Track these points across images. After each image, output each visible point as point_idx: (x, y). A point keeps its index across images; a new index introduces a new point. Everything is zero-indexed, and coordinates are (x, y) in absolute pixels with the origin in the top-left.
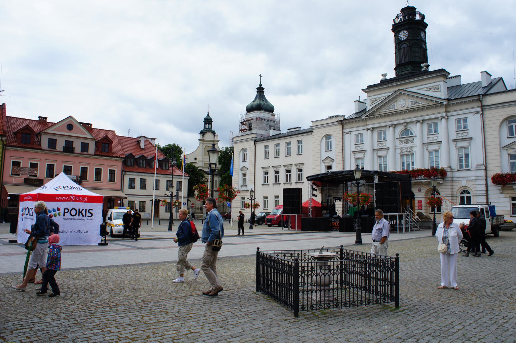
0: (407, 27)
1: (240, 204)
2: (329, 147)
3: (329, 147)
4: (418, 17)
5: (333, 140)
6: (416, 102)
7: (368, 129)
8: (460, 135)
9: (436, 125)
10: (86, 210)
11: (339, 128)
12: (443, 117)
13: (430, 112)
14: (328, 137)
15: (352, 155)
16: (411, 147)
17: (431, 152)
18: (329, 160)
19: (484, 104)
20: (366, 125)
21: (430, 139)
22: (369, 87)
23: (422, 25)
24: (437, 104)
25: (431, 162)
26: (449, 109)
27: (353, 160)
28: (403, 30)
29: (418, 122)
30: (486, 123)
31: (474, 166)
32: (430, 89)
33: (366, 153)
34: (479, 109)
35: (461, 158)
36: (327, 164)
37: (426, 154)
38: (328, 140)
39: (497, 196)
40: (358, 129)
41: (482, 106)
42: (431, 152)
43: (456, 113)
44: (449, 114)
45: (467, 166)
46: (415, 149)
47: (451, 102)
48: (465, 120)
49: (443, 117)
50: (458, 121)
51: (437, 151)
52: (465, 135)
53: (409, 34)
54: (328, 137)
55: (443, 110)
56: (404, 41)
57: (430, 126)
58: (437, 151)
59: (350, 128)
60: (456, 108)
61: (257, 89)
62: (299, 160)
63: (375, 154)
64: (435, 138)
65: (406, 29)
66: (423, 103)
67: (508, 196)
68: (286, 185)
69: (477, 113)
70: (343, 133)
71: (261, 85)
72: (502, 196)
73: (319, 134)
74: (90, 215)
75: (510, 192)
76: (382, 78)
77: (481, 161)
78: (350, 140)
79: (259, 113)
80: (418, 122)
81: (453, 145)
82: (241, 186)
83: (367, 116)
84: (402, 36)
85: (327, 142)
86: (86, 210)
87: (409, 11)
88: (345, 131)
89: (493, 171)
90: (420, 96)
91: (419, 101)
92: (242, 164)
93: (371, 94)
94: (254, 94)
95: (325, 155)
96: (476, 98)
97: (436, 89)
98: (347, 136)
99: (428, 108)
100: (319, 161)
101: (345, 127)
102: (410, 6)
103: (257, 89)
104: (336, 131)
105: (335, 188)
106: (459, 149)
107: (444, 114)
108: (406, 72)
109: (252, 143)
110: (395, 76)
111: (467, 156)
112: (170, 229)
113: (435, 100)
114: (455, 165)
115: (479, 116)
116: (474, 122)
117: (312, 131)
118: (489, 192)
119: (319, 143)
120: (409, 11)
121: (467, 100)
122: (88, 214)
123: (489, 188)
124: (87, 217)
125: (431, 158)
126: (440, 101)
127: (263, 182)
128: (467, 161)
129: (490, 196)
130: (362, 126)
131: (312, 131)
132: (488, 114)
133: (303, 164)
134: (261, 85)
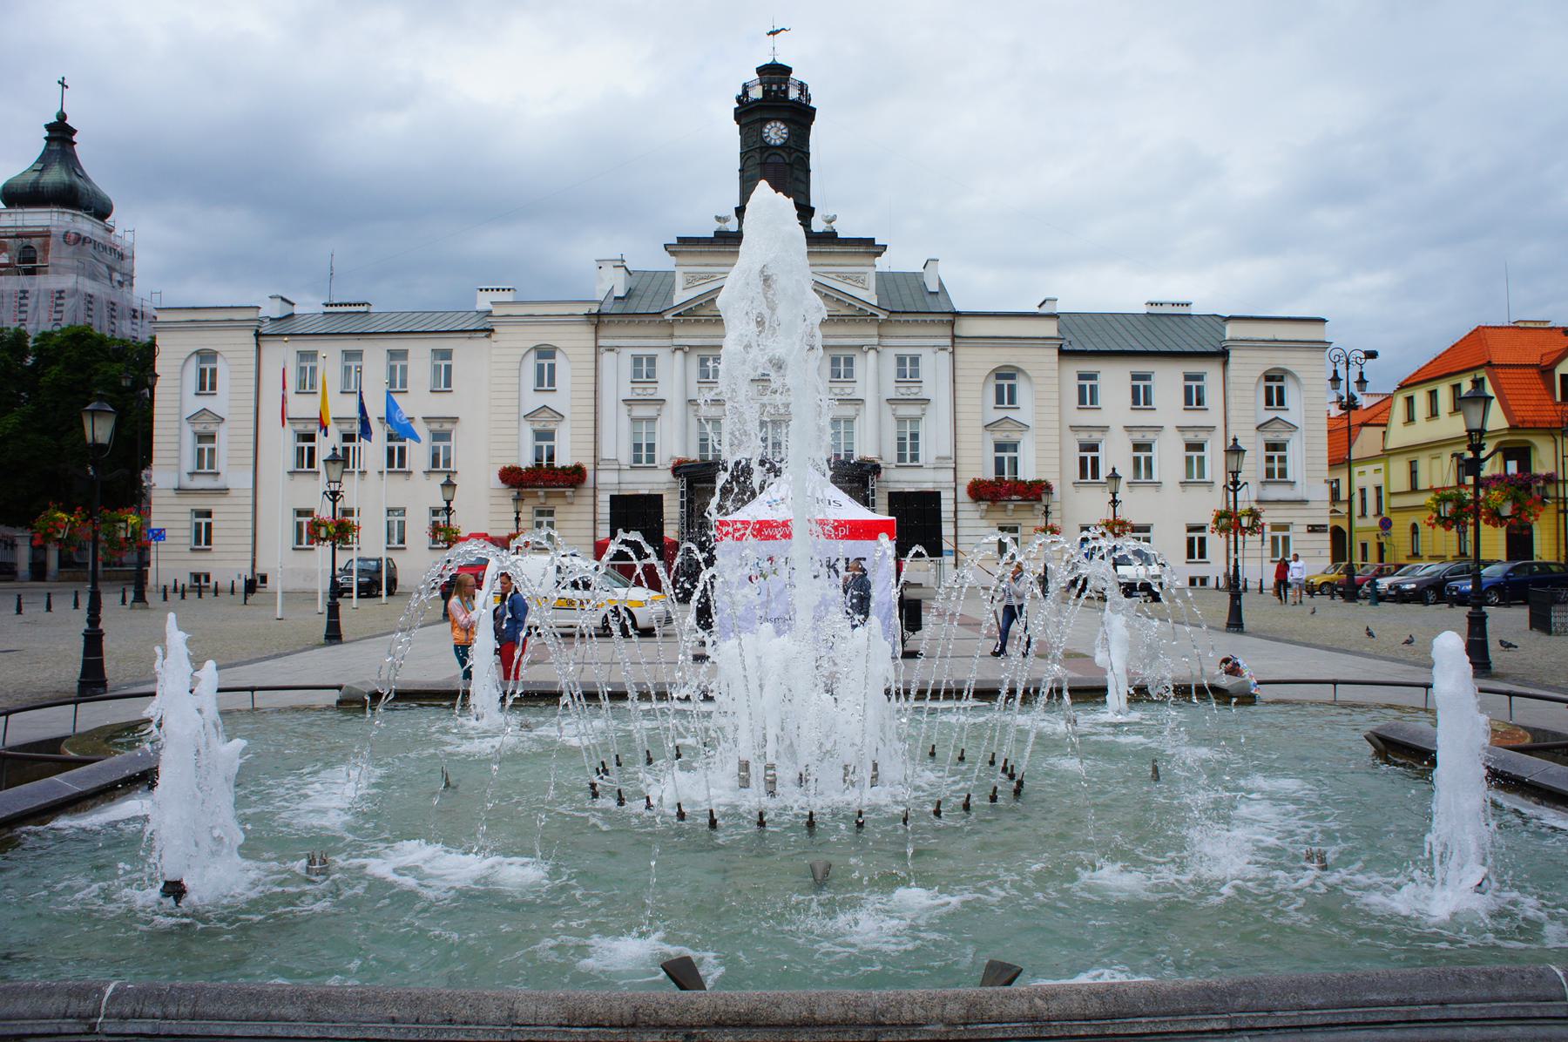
0: (786, 115)
1: (187, 533)
3: (546, 379)
4: (793, 94)
5: (220, 365)
7: (680, 348)
9: (849, 361)
14: (207, 356)
15: (624, 408)
19: (957, 332)
20: (671, 336)
22: (683, 241)
23: (801, 115)
26: (885, 331)
27: (625, 423)
28: (776, 120)
30: (958, 372)
31: (932, 459)
32: (845, 278)
33: (665, 409)
34: (948, 342)
35: (901, 439)
36: (538, 426)
41: (954, 337)
43: (904, 342)
44: (886, 341)
45: (915, 457)
48: (915, 360)
49: (872, 348)
53: (789, 133)
54: (545, 352)
55: (873, 331)
61: (49, 127)
62: (441, 406)
63: (691, 414)
65: (783, 121)
68: (197, 478)
69: (943, 349)
70: (597, 347)
71: (62, 117)
72: (984, 523)
73: (514, 343)
76: (717, 226)
77: (947, 451)
79: (68, 218)
81: (887, 408)
82: (192, 474)
83: (679, 315)
84: (772, 134)
87: (775, 74)
92: (194, 404)
93: (683, 260)
94: (36, 143)
95: (533, 401)
97: (858, 280)
98: (607, 359)
100: (515, 417)
101: (601, 333)
102: (779, 61)
103: (49, 127)
104: (574, 344)
105: (569, 491)
107: (875, 341)
109: (249, 337)
111: (915, 436)
112: (76, 605)
114: (890, 454)
115: (945, 356)
116: (934, 366)
117: (489, 331)
118: (960, 515)
120: (775, 74)
121: (929, 318)
123: (960, 507)
125: (836, 435)
126: (870, 311)
127: (291, 466)
128: (915, 447)
129: (960, 523)
132: (963, 353)
133: (455, 420)
134: (62, 117)
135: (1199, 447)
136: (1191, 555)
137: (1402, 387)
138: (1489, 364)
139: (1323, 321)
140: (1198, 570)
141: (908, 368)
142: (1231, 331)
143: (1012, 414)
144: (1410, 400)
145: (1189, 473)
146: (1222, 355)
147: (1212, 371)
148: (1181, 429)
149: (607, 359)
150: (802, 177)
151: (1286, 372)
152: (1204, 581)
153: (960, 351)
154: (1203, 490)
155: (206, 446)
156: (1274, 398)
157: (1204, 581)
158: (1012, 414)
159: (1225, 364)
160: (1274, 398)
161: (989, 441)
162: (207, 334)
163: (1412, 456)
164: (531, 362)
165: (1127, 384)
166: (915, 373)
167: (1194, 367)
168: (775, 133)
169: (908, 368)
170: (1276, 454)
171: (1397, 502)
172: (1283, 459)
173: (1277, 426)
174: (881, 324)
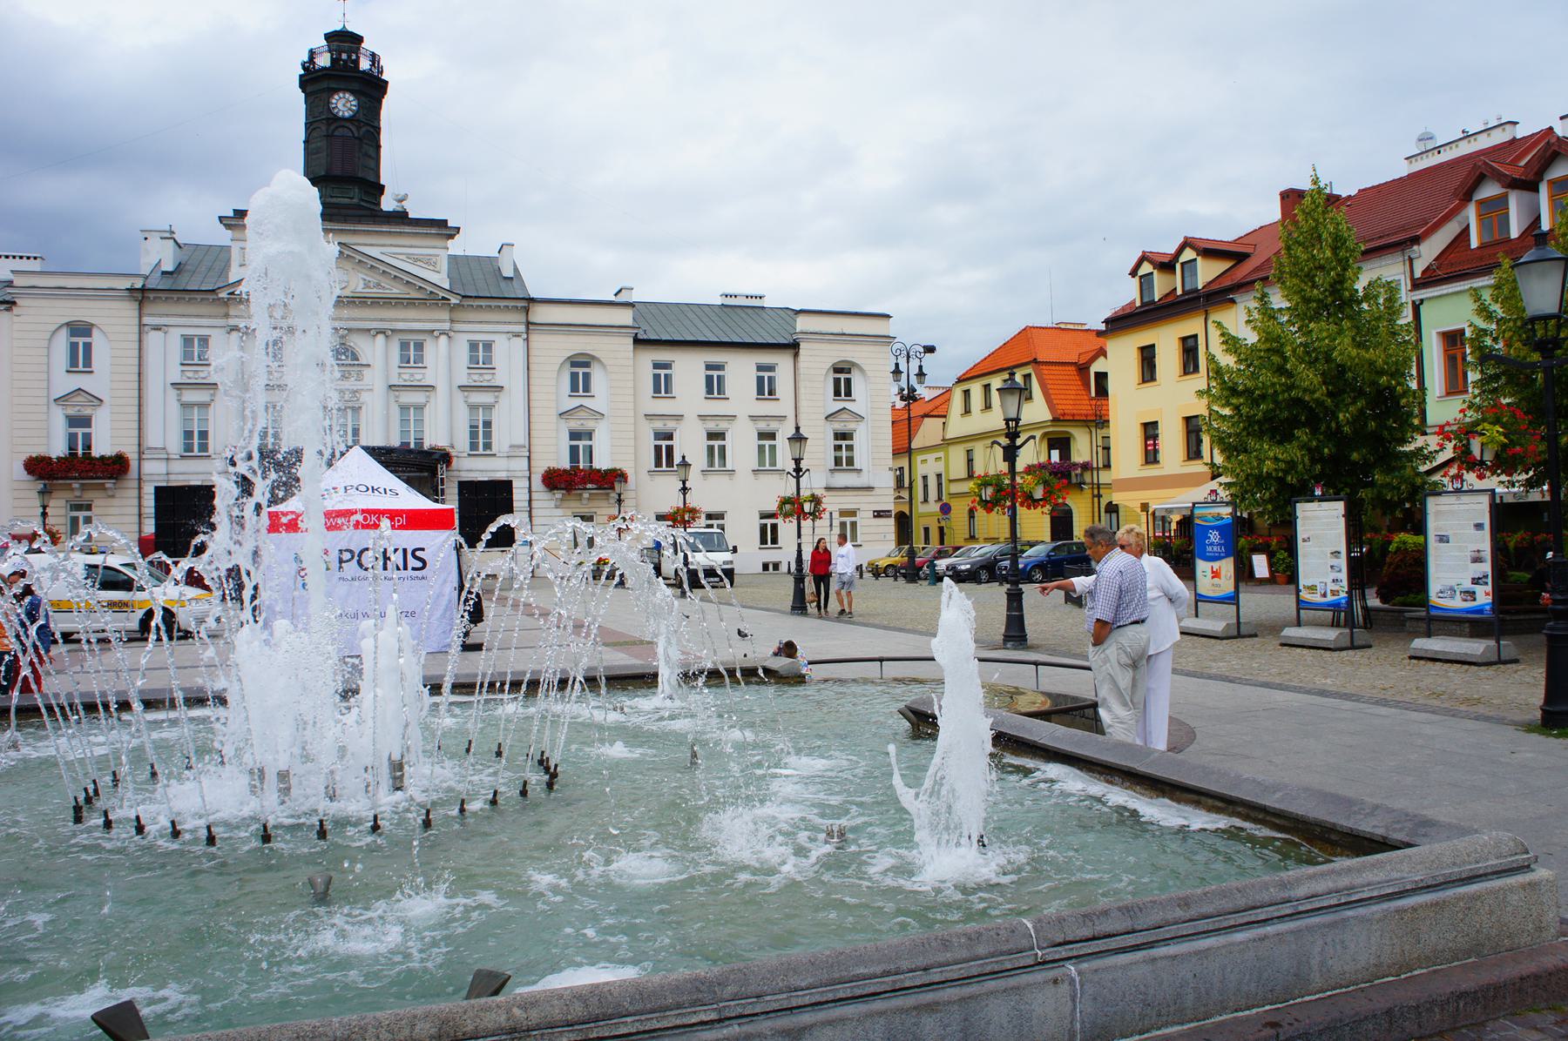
2: (80, 359)
3: (80, 359)
5: (97, 339)
6: (378, 285)
8: (476, 377)
10: (405, 551)
11: (128, 310)
12: (443, 333)
13: (411, 313)
14: (80, 329)
15: (172, 393)
16: (355, 392)
17: (404, 408)
18: (80, 399)
20: (227, 316)
21: (406, 377)
23: (372, 88)
24: (431, 299)
25: (404, 433)
27: (174, 409)
28: (345, 90)
29: (382, 332)
31: (505, 448)
32: (416, 260)
34: (522, 328)
35: (474, 427)
36: (71, 411)
37: (395, 411)
38: (75, 339)
39: (547, 512)
40: (196, 321)
41: (528, 324)
42: (404, 408)
43: (478, 327)
44: (458, 327)
45: (488, 446)
46: (365, 397)
47: (467, 302)
48: (488, 346)
49: (443, 333)
50: (473, 346)
51: (420, 408)
52: (486, 379)
53: (359, 105)
54: (80, 329)
55: (445, 315)
56: (343, 119)
57: (404, 346)
58: (420, 408)
59: (161, 315)
60: (472, 316)
64: (418, 377)
65: (352, 92)
66: (396, 290)
67: (63, 503)
70: (141, 325)
72: (559, 512)
74: (420, 564)
75: (576, 504)
77: (521, 439)
78: (165, 351)
80: (382, 332)
85: (74, 347)
86: (405, 551)
87: (344, 41)
88: (146, 320)
89: (542, 465)
90: (382, 268)
91: (385, 282)
95: (65, 383)
96: (521, 304)
97: (429, 262)
98: (153, 338)
99: (410, 303)
101: (146, 310)
105: (109, 484)
106: (473, 408)
107: (446, 326)
108: (346, 201)
110: (1339, 507)
111: (488, 424)
113: (430, 289)
114: (462, 444)
115: (519, 342)
116: (508, 353)
118: (534, 504)
119: (45, 343)
120: (344, 41)
122: (412, 563)
123: (535, 496)
124: (410, 572)
125: (404, 421)
128: (488, 435)
130: (210, 317)
131: (14, 303)
132: (536, 339)
135: (719, 435)
136: (763, 541)
137: (960, 381)
138: (1035, 361)
139: (888, 316)
140: (771, 556)
141: (480, 354)
142: (802, 324)
143: (848, 405)
144: (967, 393)
145: (711, 463)
146: (793, 347)
147: (783, 362)
148: (702, 417)
149: (153, 338)
150: (371, 152)
151: (854, 364)
152: (776, 566)
153: (534, 338)
154: (724, 479)
155: (716, 443)
156: (842, 389)
157: (776, 566)
158: (848, 405)
159: (796, 355)
160: (842, 389)
161: (564, 428)
162: (849, 347)
163: (969, 446)
164: (63, 340)
165: (700, 375)
166: (419, 359)
167: (766, 358)
168: (344, 104)
169: (480, 354)
170: (844, 443)
171: (955, 488)
172: (850, 448)
173: (844, 416)
174: (453, 308)
